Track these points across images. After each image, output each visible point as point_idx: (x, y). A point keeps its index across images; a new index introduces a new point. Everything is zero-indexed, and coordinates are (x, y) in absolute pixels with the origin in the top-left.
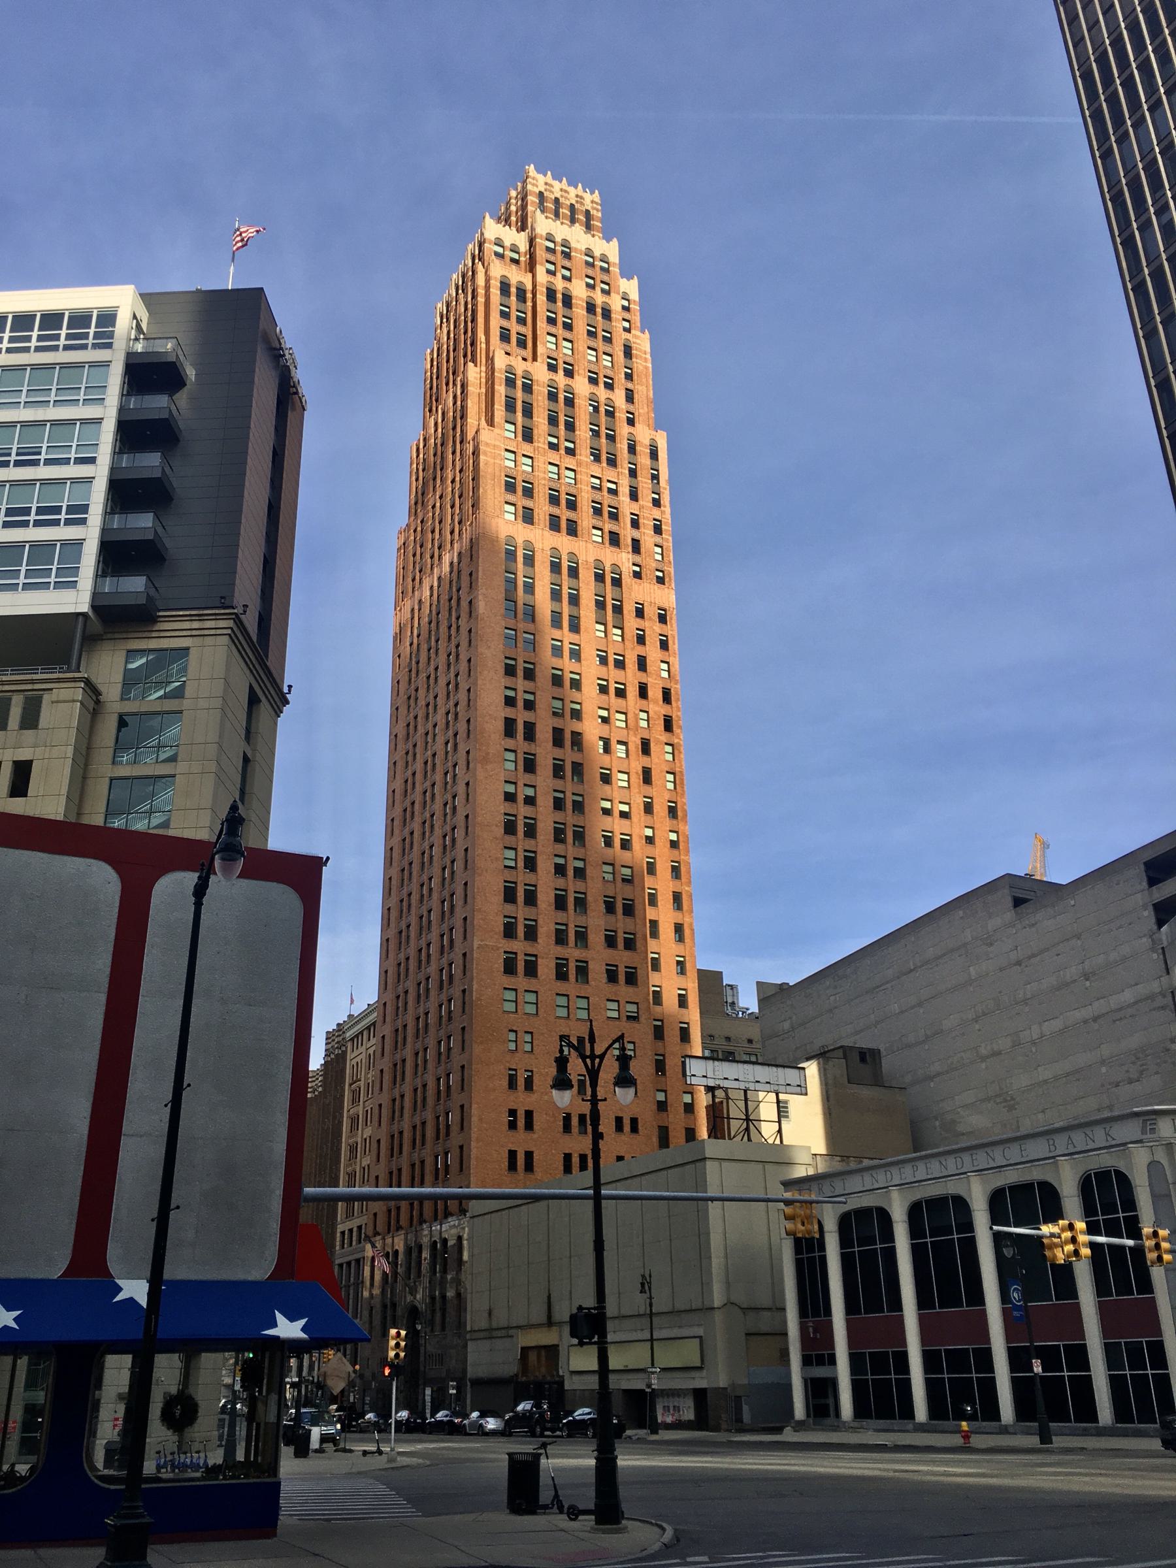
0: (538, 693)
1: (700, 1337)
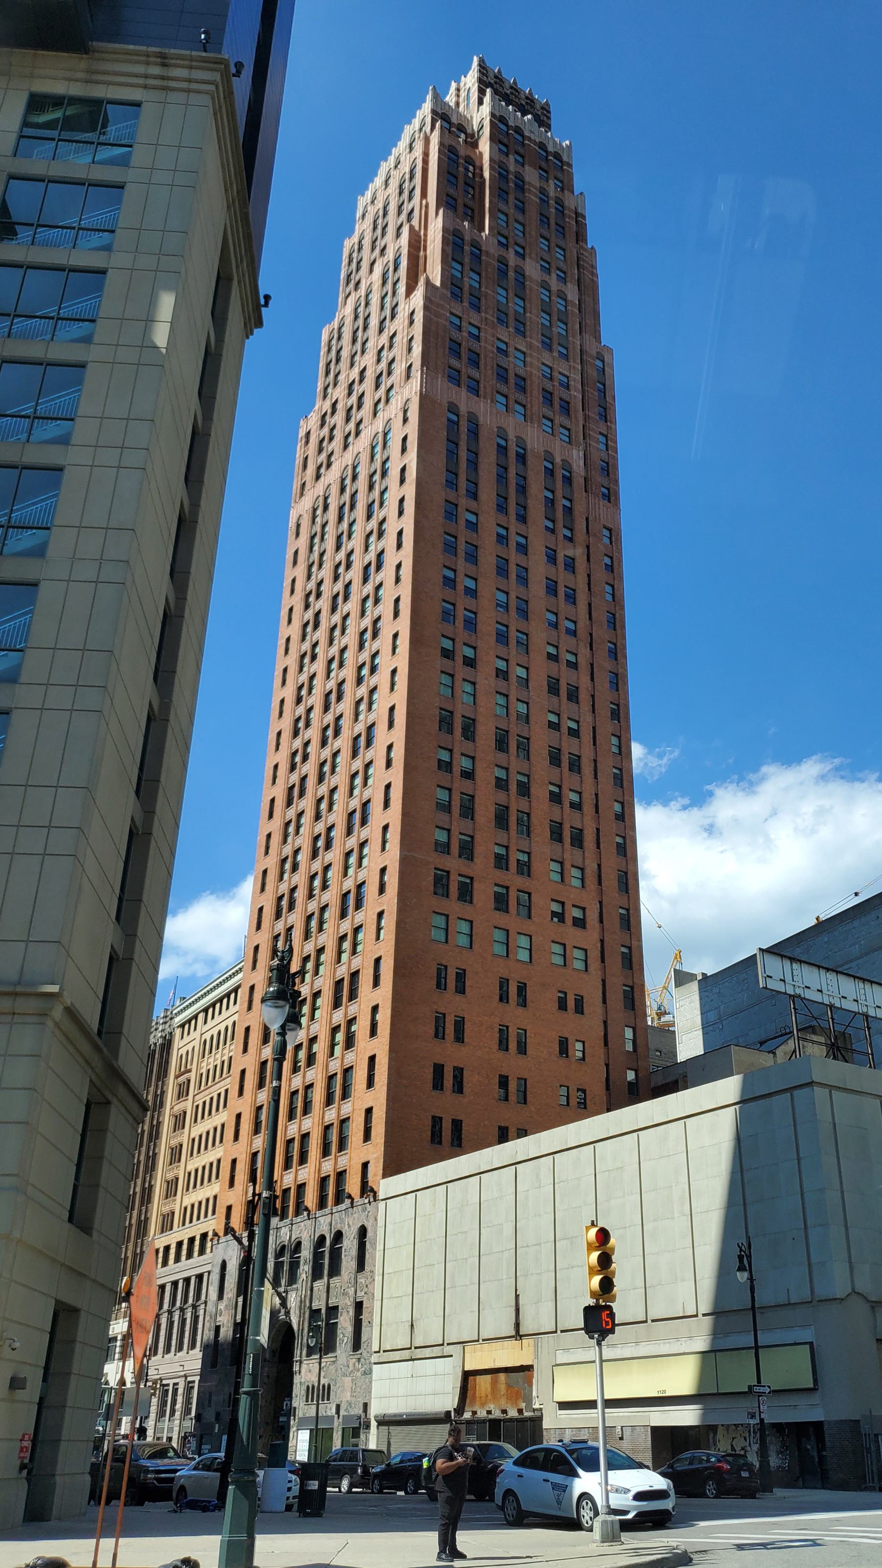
0: (480, 580)
1: (811, 1344)
